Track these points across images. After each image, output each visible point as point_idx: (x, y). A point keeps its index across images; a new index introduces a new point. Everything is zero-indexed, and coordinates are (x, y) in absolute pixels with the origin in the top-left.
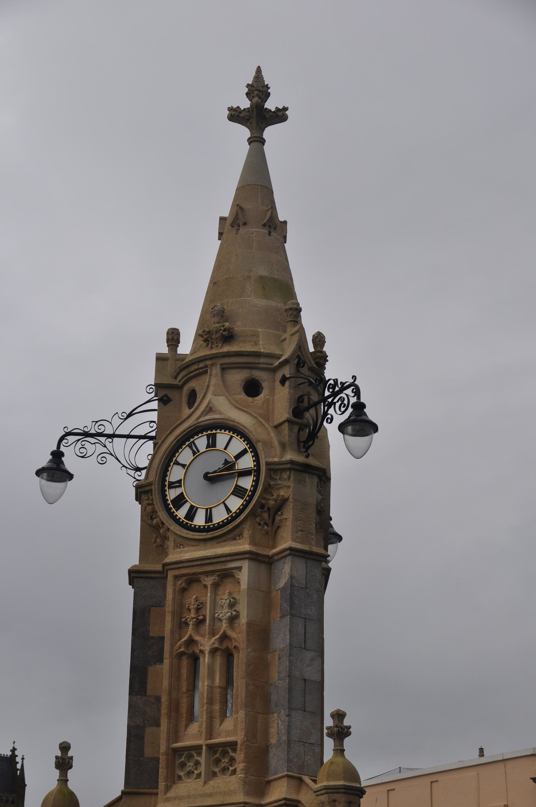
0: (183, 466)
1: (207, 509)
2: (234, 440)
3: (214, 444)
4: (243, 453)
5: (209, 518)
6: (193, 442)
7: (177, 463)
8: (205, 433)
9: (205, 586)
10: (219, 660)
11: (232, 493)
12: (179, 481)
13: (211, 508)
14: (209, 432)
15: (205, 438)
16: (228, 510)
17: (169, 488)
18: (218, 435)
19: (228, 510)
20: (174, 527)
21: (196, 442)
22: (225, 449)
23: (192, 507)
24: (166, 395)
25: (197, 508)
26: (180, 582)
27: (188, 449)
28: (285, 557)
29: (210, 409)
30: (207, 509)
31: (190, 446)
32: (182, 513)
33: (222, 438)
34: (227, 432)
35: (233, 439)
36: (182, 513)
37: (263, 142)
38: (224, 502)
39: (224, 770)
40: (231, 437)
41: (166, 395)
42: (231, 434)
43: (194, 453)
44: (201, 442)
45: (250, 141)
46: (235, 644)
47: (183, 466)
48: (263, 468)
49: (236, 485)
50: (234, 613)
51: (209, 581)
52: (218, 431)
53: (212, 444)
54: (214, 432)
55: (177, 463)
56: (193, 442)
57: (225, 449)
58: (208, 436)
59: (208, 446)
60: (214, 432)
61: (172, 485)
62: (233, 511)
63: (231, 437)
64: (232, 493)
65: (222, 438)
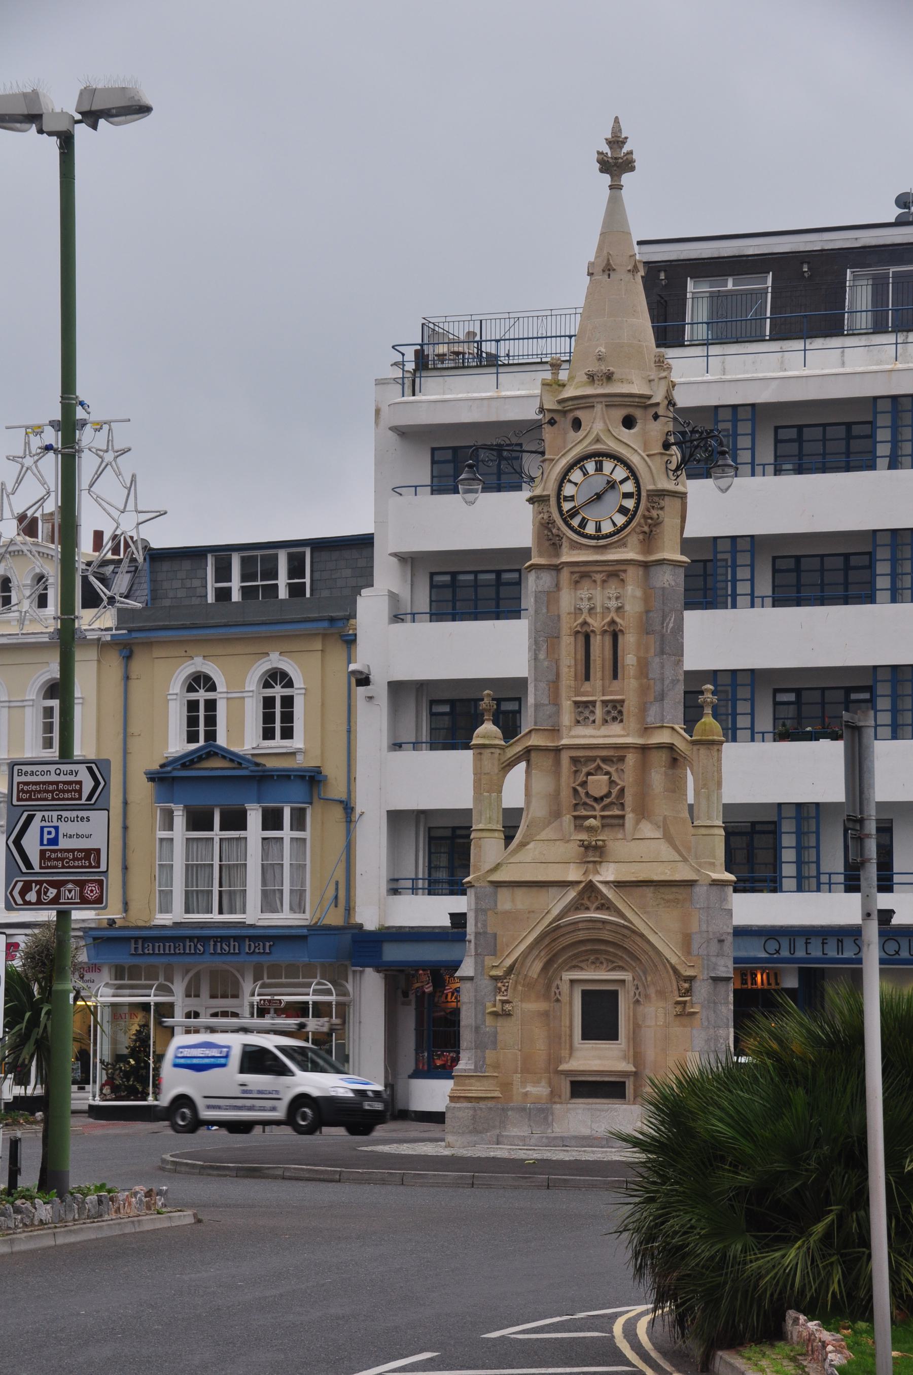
0: (576, 484)
1: (596, 522)
2: (617, 468)
3: (601, 470)
4: (626, 479)
5: (598, 529)
6: (583, 465)
7: (570, 481)
8: (593, 459)
9: (595, 581)
10: (608, 640)
11: (618, 511)
12: (573, 497)
13: (600, 521)
14: (597, 459)
15: (594, 463)
16: (614, 524)
17: (564, 501)
18: (604, 462)
19: (614, 524)
20: (570, 534)
21: (586, 465)
22: (611, 474)
23: (584, 519)
24: (552, 418)
25: (600, 521)
26: (574, 577)
27: (579, 470)
28: (840, 598)
29: (598, 440)
30: (596, 522)
31: (581, 468)
32: (575, 522)
33: (608, 466)
34: (612, 460)
35: (617, 467)
36: (575, 522)
37: (620, 187)
38: (611, 518)
39: (614, 719)
40: (616, 465)
41: (552, 418)
42: (616, 462)
43: (585, 475)
44: (590, 466)
45: (611, 187)
46: (591, 628)
47: (576, 484)
48: (644, 494)
49: (621, 505)
50: (620, 605)
51: (599, 577)
52: (605, 459)
53: (599, 469)
54: (601, 458)
55: (570, 481)
56: (583, 465)
57: (611, 474)
58: (596, 462)
59: (596, 470)
60: (601, 458)
61: (567, 499)
62: (619, 525)
63: (616, 465)
64: (618, 511)
65: (608, 466)
